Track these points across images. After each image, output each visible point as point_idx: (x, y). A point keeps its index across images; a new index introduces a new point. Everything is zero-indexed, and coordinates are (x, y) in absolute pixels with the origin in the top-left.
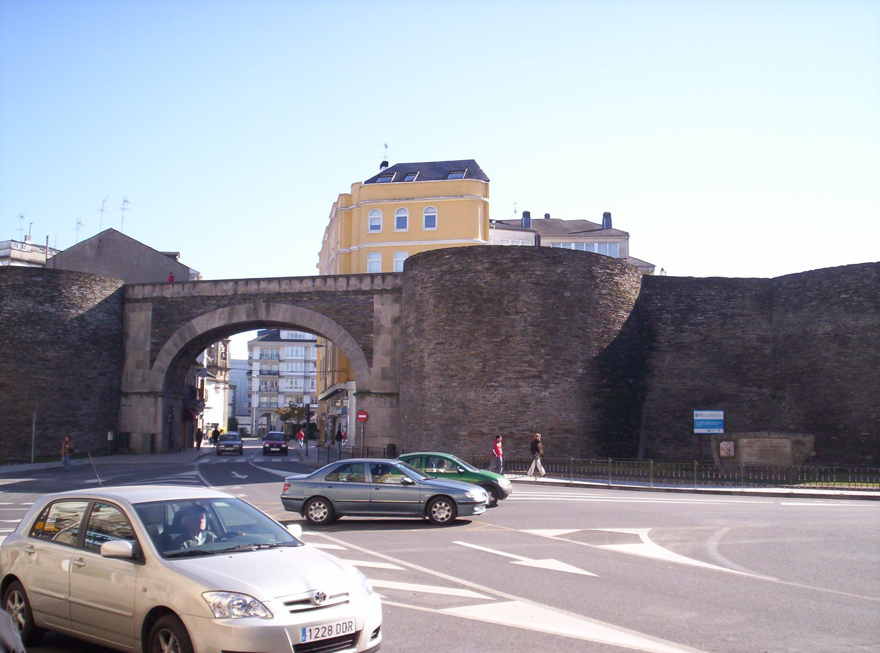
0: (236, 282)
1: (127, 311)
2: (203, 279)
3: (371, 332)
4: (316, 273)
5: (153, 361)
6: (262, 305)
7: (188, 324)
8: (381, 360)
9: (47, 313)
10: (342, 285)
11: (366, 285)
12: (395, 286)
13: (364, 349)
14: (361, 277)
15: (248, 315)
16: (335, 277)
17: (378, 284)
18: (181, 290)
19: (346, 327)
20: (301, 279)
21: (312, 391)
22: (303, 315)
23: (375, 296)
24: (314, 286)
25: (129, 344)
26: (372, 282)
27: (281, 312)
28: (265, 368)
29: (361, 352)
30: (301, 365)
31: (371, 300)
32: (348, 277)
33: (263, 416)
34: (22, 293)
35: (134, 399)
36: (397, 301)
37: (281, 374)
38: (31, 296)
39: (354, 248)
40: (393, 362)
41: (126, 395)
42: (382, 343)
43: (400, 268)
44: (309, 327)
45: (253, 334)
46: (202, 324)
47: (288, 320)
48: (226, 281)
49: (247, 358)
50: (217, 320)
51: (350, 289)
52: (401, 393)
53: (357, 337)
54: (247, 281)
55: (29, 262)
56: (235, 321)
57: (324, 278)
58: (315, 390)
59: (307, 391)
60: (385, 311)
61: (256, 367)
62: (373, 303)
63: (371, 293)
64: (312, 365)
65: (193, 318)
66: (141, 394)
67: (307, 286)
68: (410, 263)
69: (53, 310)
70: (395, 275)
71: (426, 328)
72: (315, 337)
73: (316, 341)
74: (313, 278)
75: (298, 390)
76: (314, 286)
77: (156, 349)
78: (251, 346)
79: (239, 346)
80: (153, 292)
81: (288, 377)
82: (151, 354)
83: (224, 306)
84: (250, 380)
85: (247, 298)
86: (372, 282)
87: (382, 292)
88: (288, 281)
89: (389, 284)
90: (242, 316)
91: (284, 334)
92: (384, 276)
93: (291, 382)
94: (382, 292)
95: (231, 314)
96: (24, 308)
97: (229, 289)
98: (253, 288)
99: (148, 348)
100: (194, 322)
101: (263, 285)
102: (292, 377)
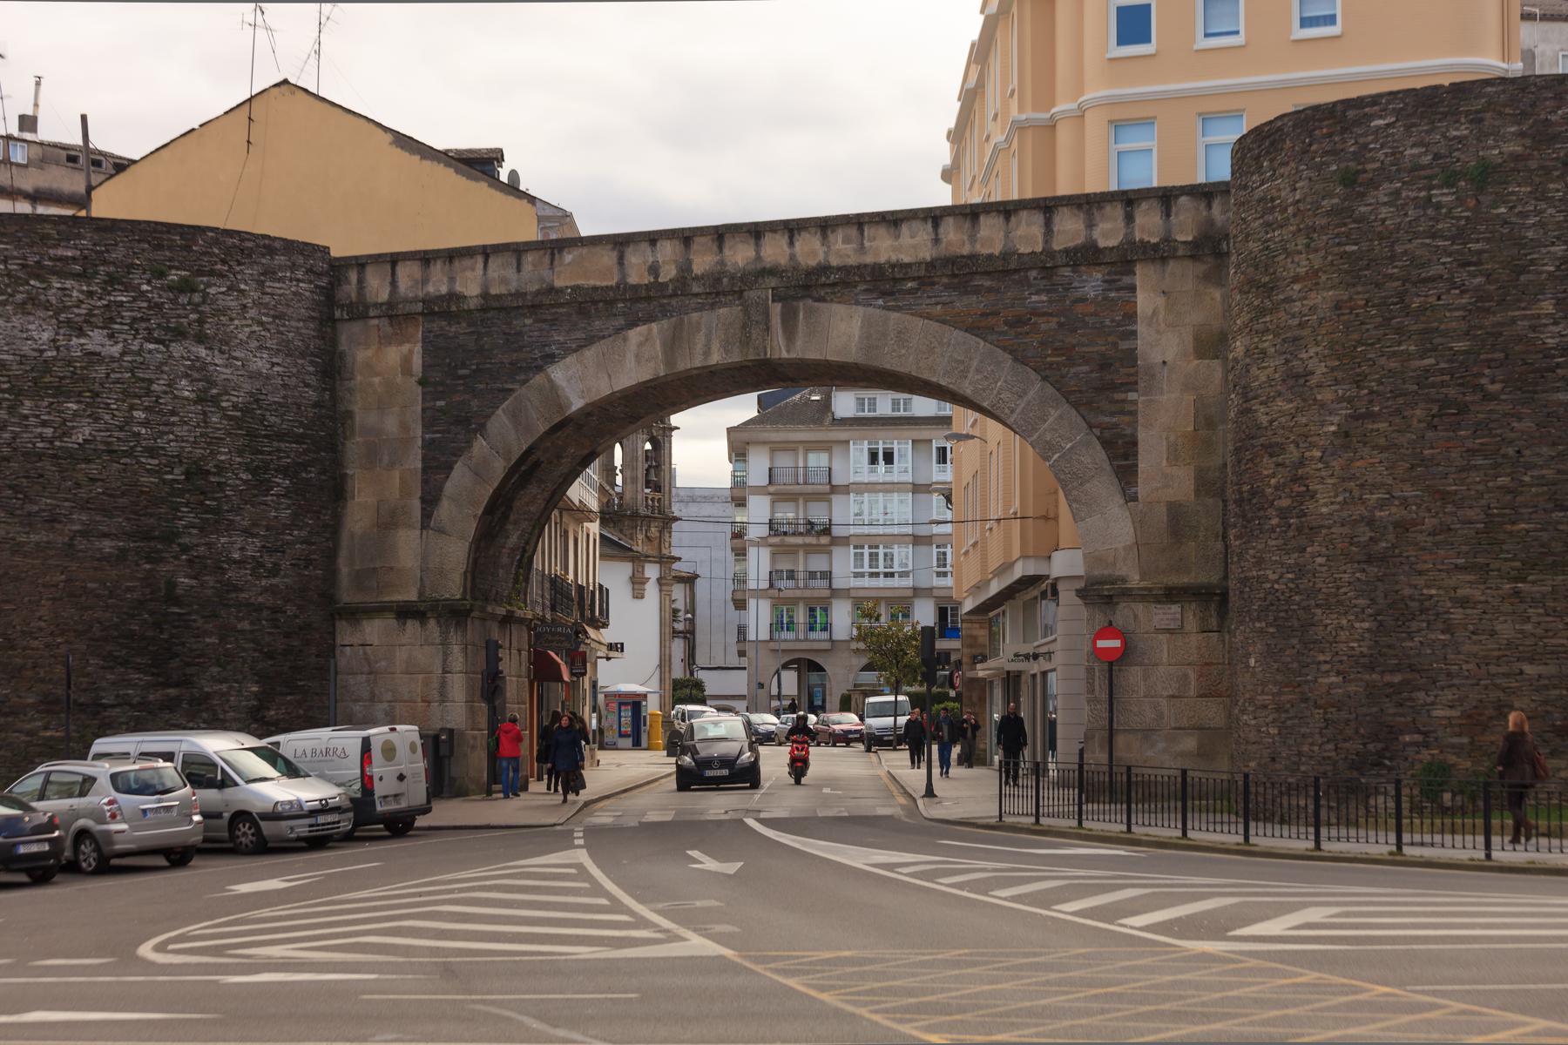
0: (685, 237)
1: (343, 344)
2: (585, 231)
3: (1132, 386)
4: (941, 196)
5: (430, 501)
6: (770, 304)
7: (538, 379)
8: (1164, 473)
9: (93, 357)
10: (1028, 235)
11: (1109, 232)
12: (1201, 232)
13: (1107, 444)
14: (1088, 204)
15: (726, 347)
16: (1007, 210)
17: (1148, 224)
18: (511, 273)
19: (1047, 373)
20: (893, 220)
21: (938, 582)
22: (915, 337)
23: (1138, 269)
24: (937, 241)
25: (354, 448)
26: (1129, 218)
27: (843, 329)
28: (787, 513)
29: (1101, 455)
30: (933, 499)
31: (1126, 280)
32: (1047, 207)
33: (785, 666)
34: (19, 297)
35: (374, 630)
36: (1215, 277)
37: (837, 531)
38: (47, 306)
39: (1061, 107)
40: (1204, 484)
41: (356, 614)
42: (1163, 420)
43: (1222, 170)
44: (926, 376)
45: (742, 408)
46: (578, 380)
47: (853, 355)
48: (653, 238)
49: (727, 483)
50: (633, 359)
51: (1057, 246)
52: (1232, 584)
53: (1081, 401)
54: (721, 234)
55: (36, 197)
56: (683, 365)
57: (970, 214)
58: (948, 582)
59: (924, 584)
60: (1165, 323)
61: (758, 511)
62: (1133, 289)
63: (1126, 258)
64: (937, 500)
65: (551, 358)
66: (405, 612)
67: (914, 246)
68: (1258, 147)
69: (116, 350)
70: (1205, 193)
71: (1311, 364)
72: (948, 409)
73: (946, 421)
74: (934, 216)
75: (896, 582)
76: (937, 241)
77: (437, 465)
78: (740, 443)
79: (700, 445)
80: (425, 281)
81: (858, 542)
82: (425, 482)
83: (650, 319)
84: (740, 553)
85: (723, 289)
86: (1129, 218)
87: (1160, 253)
88: (853, 232)
89: (1186, 224)
90: (710, 346)
91: (845, 403)
92: (1165, 197)
93: (874, 557)
94: (1160, 253)
95: (673, 344)
96: (27, 348)
97: (600, 272)
98: (740, 255)
99: (415, 462)
100: (558, 373)
101: (637, 260)
102: (873, 542)
